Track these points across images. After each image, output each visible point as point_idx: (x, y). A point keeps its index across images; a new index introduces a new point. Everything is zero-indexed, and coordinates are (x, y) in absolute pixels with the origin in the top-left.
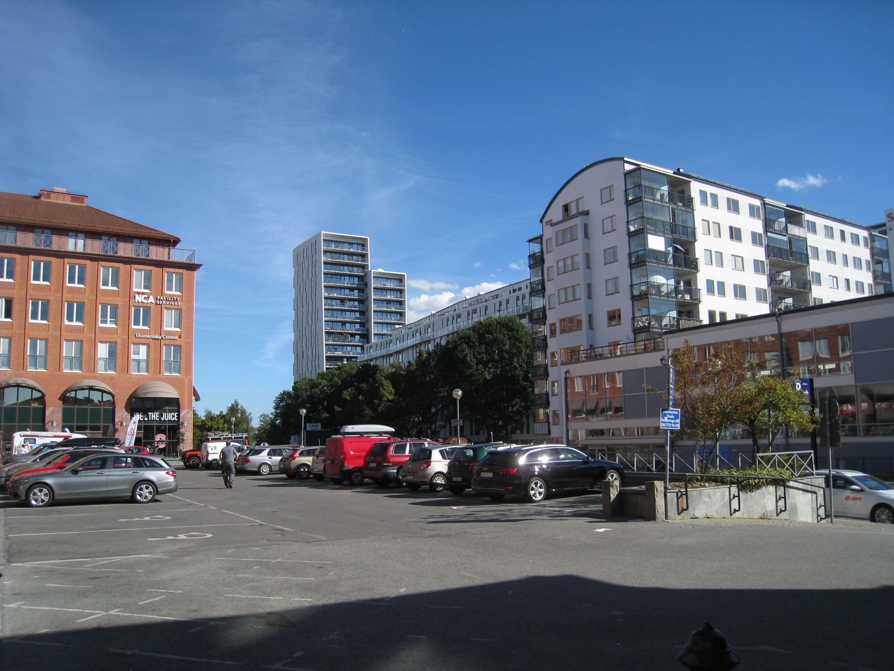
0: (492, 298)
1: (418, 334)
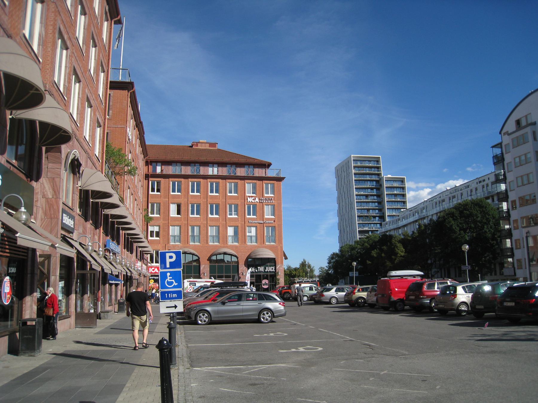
0: (465, 187)
1: (416, 214)
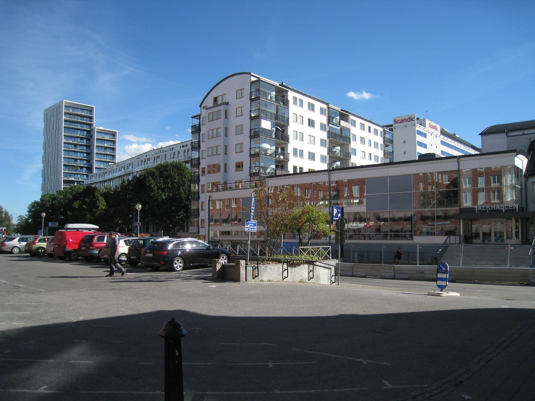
1: (123, 169)
